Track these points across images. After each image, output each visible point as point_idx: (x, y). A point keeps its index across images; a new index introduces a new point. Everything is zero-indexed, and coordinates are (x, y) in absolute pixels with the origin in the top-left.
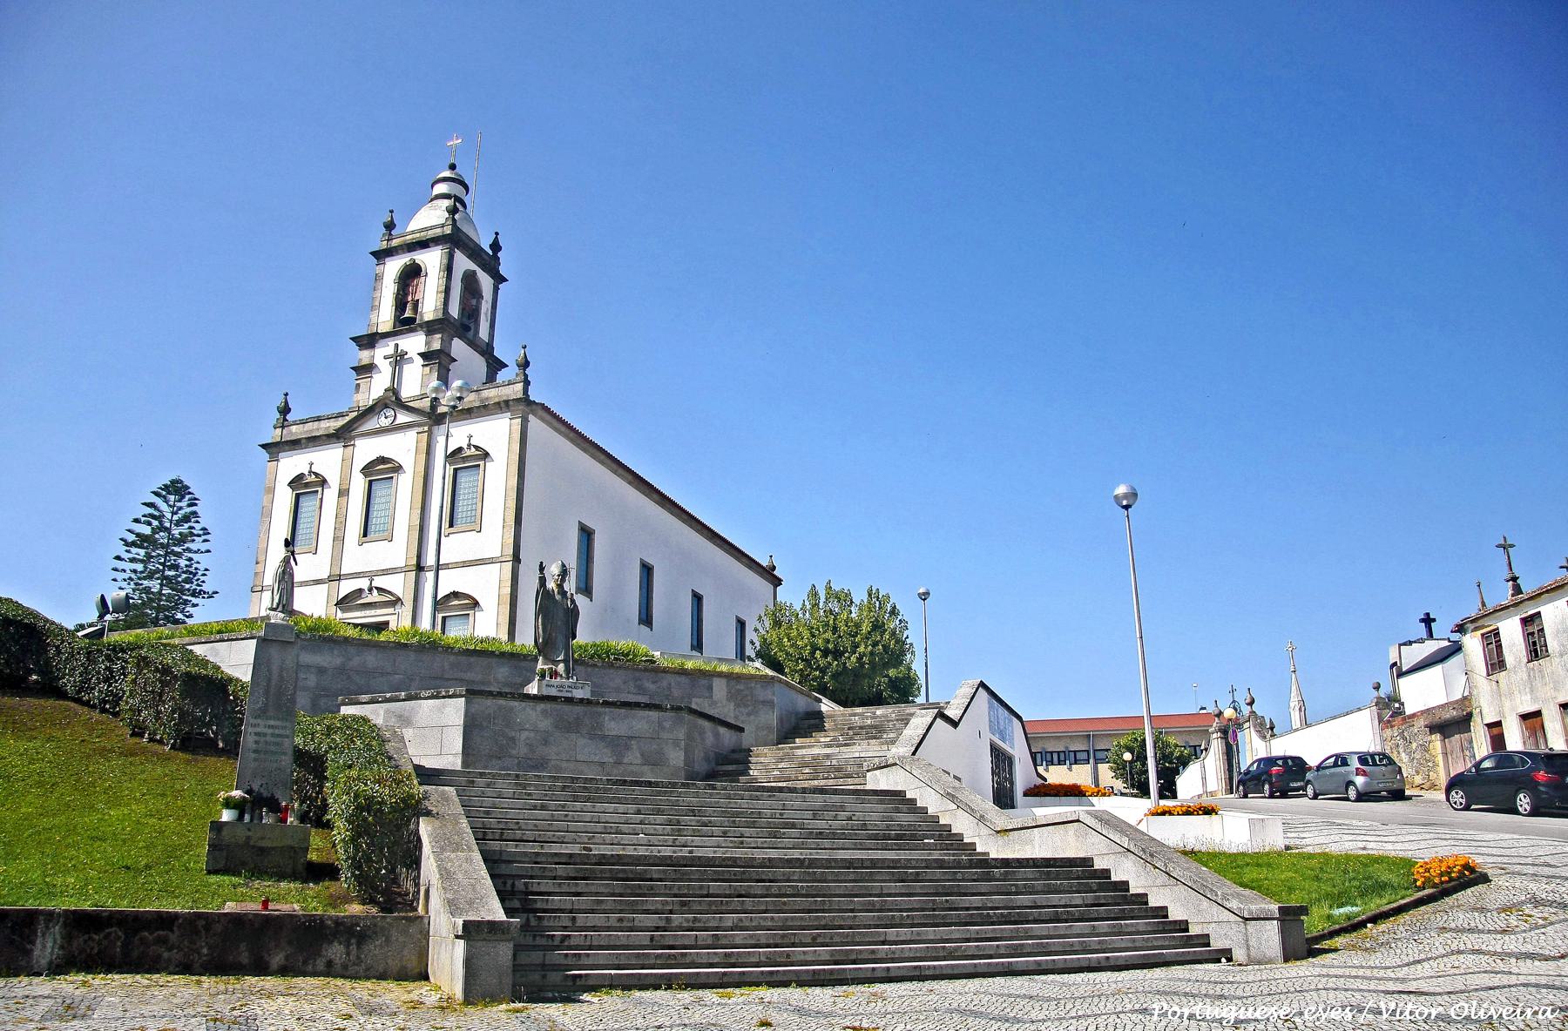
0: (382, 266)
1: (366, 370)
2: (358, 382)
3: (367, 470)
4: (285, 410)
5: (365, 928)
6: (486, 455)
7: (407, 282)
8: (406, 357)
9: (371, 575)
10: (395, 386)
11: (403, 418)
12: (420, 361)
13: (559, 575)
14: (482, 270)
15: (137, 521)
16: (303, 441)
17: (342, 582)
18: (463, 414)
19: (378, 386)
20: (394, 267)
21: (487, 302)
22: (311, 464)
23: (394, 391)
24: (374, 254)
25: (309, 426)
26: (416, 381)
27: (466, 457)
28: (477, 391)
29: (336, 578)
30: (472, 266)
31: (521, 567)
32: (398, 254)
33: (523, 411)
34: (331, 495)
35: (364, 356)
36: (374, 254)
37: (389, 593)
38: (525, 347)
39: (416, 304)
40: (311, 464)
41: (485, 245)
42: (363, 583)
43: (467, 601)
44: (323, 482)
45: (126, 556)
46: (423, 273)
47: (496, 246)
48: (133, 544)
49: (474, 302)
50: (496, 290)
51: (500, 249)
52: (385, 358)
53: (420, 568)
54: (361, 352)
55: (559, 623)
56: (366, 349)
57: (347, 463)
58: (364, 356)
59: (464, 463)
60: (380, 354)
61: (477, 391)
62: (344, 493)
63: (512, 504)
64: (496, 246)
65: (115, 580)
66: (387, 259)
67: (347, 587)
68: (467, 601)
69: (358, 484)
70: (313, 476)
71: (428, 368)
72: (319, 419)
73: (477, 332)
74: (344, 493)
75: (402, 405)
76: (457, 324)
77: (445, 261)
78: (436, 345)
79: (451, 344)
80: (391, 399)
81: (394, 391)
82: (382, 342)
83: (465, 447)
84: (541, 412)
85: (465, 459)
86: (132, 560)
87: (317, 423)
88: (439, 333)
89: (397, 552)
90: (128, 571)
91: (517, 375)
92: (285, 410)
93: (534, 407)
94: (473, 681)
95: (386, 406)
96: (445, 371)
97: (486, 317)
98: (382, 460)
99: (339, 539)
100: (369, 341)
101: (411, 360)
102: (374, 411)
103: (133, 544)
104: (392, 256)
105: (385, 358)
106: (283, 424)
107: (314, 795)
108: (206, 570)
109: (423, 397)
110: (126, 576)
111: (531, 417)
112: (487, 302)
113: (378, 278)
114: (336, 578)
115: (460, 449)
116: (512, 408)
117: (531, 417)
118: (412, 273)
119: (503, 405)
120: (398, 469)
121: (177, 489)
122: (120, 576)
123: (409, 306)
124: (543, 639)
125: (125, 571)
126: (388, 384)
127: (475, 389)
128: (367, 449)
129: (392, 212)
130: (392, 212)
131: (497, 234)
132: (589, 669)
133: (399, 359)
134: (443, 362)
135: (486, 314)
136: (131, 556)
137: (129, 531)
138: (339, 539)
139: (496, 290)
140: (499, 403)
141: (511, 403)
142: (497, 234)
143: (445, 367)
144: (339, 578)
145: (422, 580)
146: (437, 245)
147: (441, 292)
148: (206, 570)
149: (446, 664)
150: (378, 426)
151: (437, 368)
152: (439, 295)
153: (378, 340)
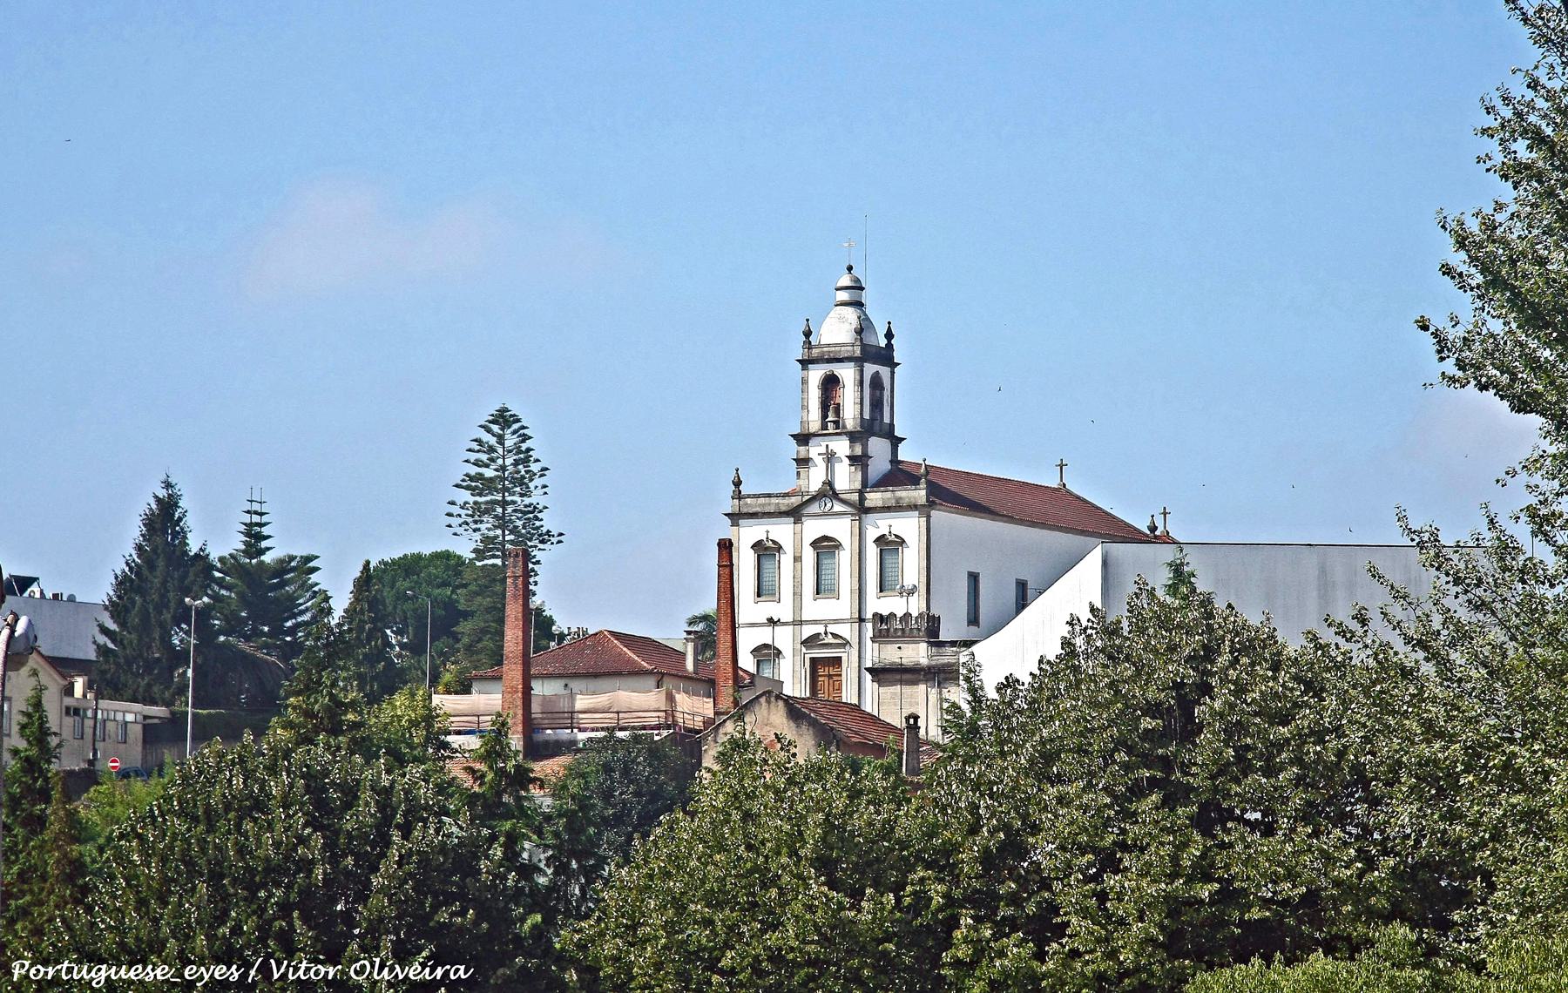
1: (803, 462)
3: (815, 544)
4: (737, 483)
5: (319, 946)
7: (829, 386)
9: (826, 623)
11: (838, 507)
12: (847, 461)
17: (804, 626)
19: (815, 479)
20: (816, 375)
22: (768, 532)
23: (829, 484)
25: (761, 500)
26: (845, 478)
29: (798, 623)
34: (786, 560)
37: (841, 637)
40: (768, 532)
42: (820, 629)
44: (779, 548)
49: (878, 393)
53: (861, 620)
57: (798, 539)
60: (815, 450)
62: (797, 559)
65: (450, 526)
67: (808, 631)
69: (809, 555)
72: (769, 496)
74: (797, 559)
75: (835, 495)
77: (858, 377)
80: (829, 491)
81: (829, 484)
89: (842, 607)
92: (737, 483)
98: (825, 538)
99: (798, 594)
100: (803, 439)
106: (738, 495)
107: (847, 776)
108: (561, 534)
109: (851, 491)
110: (460, 520)
114: (798, 623)
118: (830, 383)
120: (838, 546)
121: (503, 418)
122: (455, 521)
125: (460, 516)
126: (823, 478)
128: (814, 528)
131: (889, 323)
133: (830, 457)
138: (798, 594)
139: (893, 373)
142: (889, 323)
144: (801, 623)
145: (864, 630)
148: (561, 534)
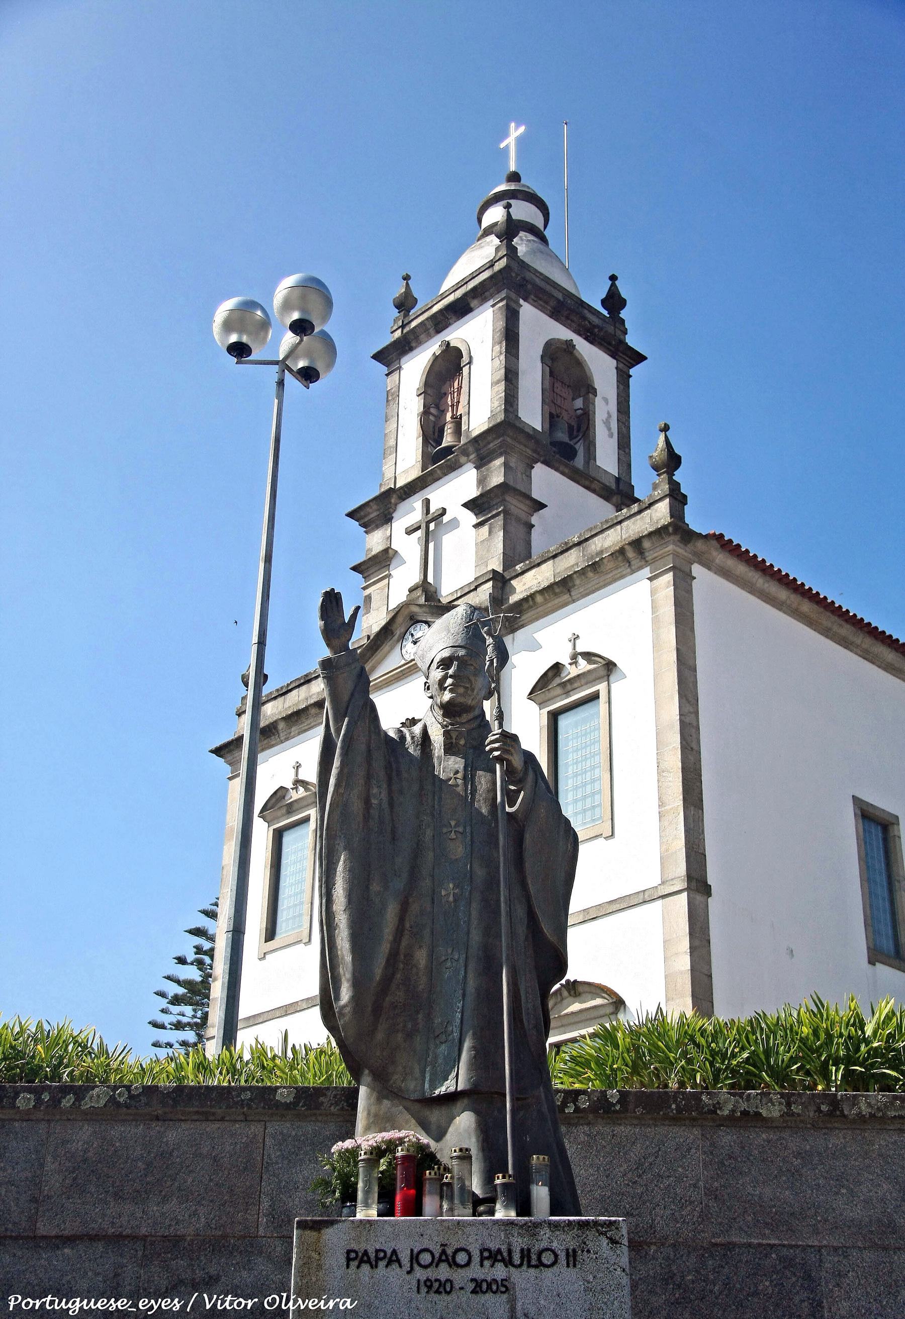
0: (395, 376)
2: (367, 592)
6: (610, 666)
8: (446, 519)
10: (430, 579)
12: (469, 518)
13: (445, 663)
14: (586, 339)
15: (181, 961)
16: (281, 725)
18: (556, 595)
21: (606, 400)
24: (379, 357)
27: (569, 680)
28: (579, 544)
30: (564, 333)
31: (714, 904)
32: (420, 343)
33: (676, 555)
35: (375, 541)
36: (379, 357)
38: (666, 428)
39: (457, 421)
40: (298, 767)
41: (594, 297)
43: (598, 1001)
45: (166, 1019)
46: (465, 359)
47: (614, 301)
48: (176, 1000)
50: (623, 379)
51: (623, 303)
52: (410, 531)
54: (370, 536)
55: (448, 890)
56: (377, 527)
58: (375, 541)
59: (567, 694)
61: (579, 544)
63: (674, 760)
64: (614, 301)
66: (403, 360)
68: (598, 1001)
70: (301, 789)
71: (486, 528)
73: (590, 454)
76: (546, 441)
77: (501, 324)
78: (497, 478)
79: (529, 477)
82: (403, 506)
83: (565, 660)
84: (721, 558)
85: (569, 685)
86: (179, 1026)
87: (304, 688)
88: (500, 455)
90: (177, 1046)
91: (655, 487)
93: (700, 545)
94: (175, 1241)
95: (414, 621)
96: (522, 530)
97: (609, 429)
101: (454, 523)
102: (392, 634)
103: (176, 1000)
104: (411, 349)
105: (410, 531)
111: (697, 570)
112: (606, 400)
113: (392, 397)
115: (557, 668)
116: (650, 556)
117: (697, 570)
119: (630, 554)
123: (448, 430)
124: (357, 984)
126: (415, 578)
127: (576, 540)
129: (407, 278)
130: (407, 278)
131: (613, 278)
132: (727, 1138)
134: (514, 510)
135: (607, 423)
136: (174, 1019)
137: (168, 978)
140: (621, 551)
141: (646, 544)
142: (613, 278)
143: (518, 520)
146: (485, 300)
147: (498, 382)
149: (50, 1165)
150: (403, 662)
151: (501, 523)
152: (496, 388)
153: (396, 505)
